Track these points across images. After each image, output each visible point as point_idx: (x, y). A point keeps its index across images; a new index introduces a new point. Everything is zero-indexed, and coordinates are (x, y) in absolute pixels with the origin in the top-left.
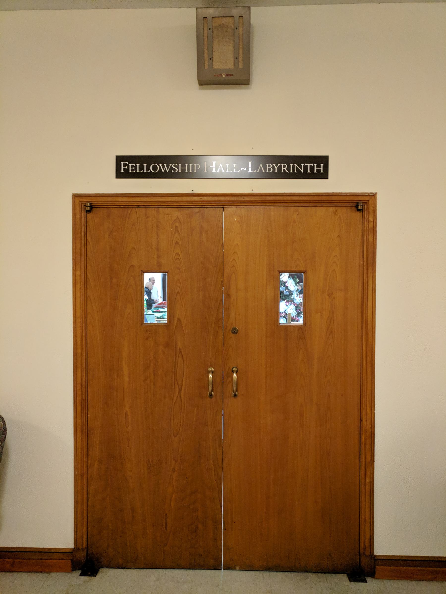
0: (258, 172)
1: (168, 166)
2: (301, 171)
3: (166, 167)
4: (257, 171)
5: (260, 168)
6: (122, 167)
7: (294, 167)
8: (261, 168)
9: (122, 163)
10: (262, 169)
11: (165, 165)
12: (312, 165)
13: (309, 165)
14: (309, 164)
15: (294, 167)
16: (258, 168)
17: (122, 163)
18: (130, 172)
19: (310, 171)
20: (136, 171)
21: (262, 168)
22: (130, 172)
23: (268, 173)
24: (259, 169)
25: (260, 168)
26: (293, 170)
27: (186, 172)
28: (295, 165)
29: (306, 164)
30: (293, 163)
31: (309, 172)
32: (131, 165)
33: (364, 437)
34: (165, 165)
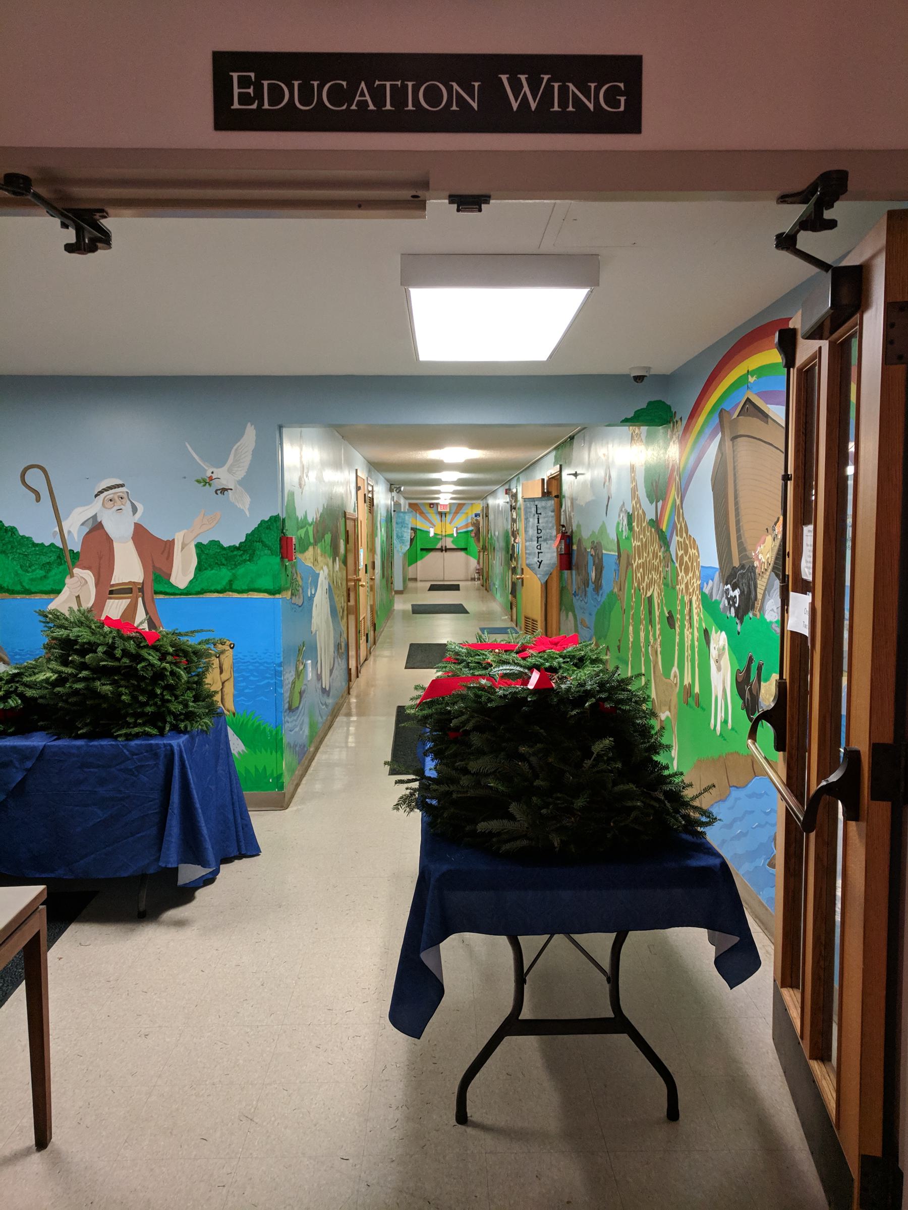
0: (354, 107)
1: (534, 87)
2: (588, 107)
3: (526, 88)
4: (350, 105)
5: (360, 96)
6: (236, 91)
7: (564, 91)
8: (362, 94)
9: (235, 75)
10: (368, 98)
11: (523, 78)
12: (399, 83)
13: (388, 84)
14: (389, 81)
15: (564, 91)
16: (355, 98)
17: (235, 75)
18: (236, 105)
19: (413, 107)
20: (261, 103)
21: (365, 96)
22: (236, 105)
23: (266, 110)
24: (357, 98)
25: (360, 96)
26: (563, 103)
27: (232, 107)
28: (568, 87)
29: (379, 81)
30: (564, 82)
31: (556, 108)
32: (391, 85)
33: (841, 881)
34: (523, 78)
